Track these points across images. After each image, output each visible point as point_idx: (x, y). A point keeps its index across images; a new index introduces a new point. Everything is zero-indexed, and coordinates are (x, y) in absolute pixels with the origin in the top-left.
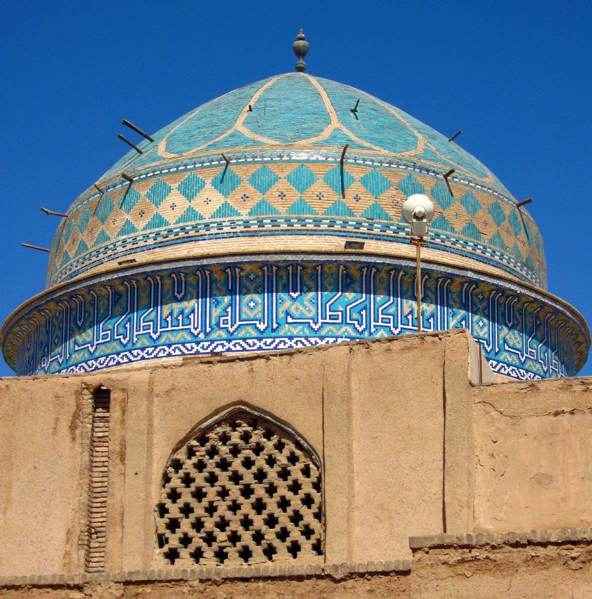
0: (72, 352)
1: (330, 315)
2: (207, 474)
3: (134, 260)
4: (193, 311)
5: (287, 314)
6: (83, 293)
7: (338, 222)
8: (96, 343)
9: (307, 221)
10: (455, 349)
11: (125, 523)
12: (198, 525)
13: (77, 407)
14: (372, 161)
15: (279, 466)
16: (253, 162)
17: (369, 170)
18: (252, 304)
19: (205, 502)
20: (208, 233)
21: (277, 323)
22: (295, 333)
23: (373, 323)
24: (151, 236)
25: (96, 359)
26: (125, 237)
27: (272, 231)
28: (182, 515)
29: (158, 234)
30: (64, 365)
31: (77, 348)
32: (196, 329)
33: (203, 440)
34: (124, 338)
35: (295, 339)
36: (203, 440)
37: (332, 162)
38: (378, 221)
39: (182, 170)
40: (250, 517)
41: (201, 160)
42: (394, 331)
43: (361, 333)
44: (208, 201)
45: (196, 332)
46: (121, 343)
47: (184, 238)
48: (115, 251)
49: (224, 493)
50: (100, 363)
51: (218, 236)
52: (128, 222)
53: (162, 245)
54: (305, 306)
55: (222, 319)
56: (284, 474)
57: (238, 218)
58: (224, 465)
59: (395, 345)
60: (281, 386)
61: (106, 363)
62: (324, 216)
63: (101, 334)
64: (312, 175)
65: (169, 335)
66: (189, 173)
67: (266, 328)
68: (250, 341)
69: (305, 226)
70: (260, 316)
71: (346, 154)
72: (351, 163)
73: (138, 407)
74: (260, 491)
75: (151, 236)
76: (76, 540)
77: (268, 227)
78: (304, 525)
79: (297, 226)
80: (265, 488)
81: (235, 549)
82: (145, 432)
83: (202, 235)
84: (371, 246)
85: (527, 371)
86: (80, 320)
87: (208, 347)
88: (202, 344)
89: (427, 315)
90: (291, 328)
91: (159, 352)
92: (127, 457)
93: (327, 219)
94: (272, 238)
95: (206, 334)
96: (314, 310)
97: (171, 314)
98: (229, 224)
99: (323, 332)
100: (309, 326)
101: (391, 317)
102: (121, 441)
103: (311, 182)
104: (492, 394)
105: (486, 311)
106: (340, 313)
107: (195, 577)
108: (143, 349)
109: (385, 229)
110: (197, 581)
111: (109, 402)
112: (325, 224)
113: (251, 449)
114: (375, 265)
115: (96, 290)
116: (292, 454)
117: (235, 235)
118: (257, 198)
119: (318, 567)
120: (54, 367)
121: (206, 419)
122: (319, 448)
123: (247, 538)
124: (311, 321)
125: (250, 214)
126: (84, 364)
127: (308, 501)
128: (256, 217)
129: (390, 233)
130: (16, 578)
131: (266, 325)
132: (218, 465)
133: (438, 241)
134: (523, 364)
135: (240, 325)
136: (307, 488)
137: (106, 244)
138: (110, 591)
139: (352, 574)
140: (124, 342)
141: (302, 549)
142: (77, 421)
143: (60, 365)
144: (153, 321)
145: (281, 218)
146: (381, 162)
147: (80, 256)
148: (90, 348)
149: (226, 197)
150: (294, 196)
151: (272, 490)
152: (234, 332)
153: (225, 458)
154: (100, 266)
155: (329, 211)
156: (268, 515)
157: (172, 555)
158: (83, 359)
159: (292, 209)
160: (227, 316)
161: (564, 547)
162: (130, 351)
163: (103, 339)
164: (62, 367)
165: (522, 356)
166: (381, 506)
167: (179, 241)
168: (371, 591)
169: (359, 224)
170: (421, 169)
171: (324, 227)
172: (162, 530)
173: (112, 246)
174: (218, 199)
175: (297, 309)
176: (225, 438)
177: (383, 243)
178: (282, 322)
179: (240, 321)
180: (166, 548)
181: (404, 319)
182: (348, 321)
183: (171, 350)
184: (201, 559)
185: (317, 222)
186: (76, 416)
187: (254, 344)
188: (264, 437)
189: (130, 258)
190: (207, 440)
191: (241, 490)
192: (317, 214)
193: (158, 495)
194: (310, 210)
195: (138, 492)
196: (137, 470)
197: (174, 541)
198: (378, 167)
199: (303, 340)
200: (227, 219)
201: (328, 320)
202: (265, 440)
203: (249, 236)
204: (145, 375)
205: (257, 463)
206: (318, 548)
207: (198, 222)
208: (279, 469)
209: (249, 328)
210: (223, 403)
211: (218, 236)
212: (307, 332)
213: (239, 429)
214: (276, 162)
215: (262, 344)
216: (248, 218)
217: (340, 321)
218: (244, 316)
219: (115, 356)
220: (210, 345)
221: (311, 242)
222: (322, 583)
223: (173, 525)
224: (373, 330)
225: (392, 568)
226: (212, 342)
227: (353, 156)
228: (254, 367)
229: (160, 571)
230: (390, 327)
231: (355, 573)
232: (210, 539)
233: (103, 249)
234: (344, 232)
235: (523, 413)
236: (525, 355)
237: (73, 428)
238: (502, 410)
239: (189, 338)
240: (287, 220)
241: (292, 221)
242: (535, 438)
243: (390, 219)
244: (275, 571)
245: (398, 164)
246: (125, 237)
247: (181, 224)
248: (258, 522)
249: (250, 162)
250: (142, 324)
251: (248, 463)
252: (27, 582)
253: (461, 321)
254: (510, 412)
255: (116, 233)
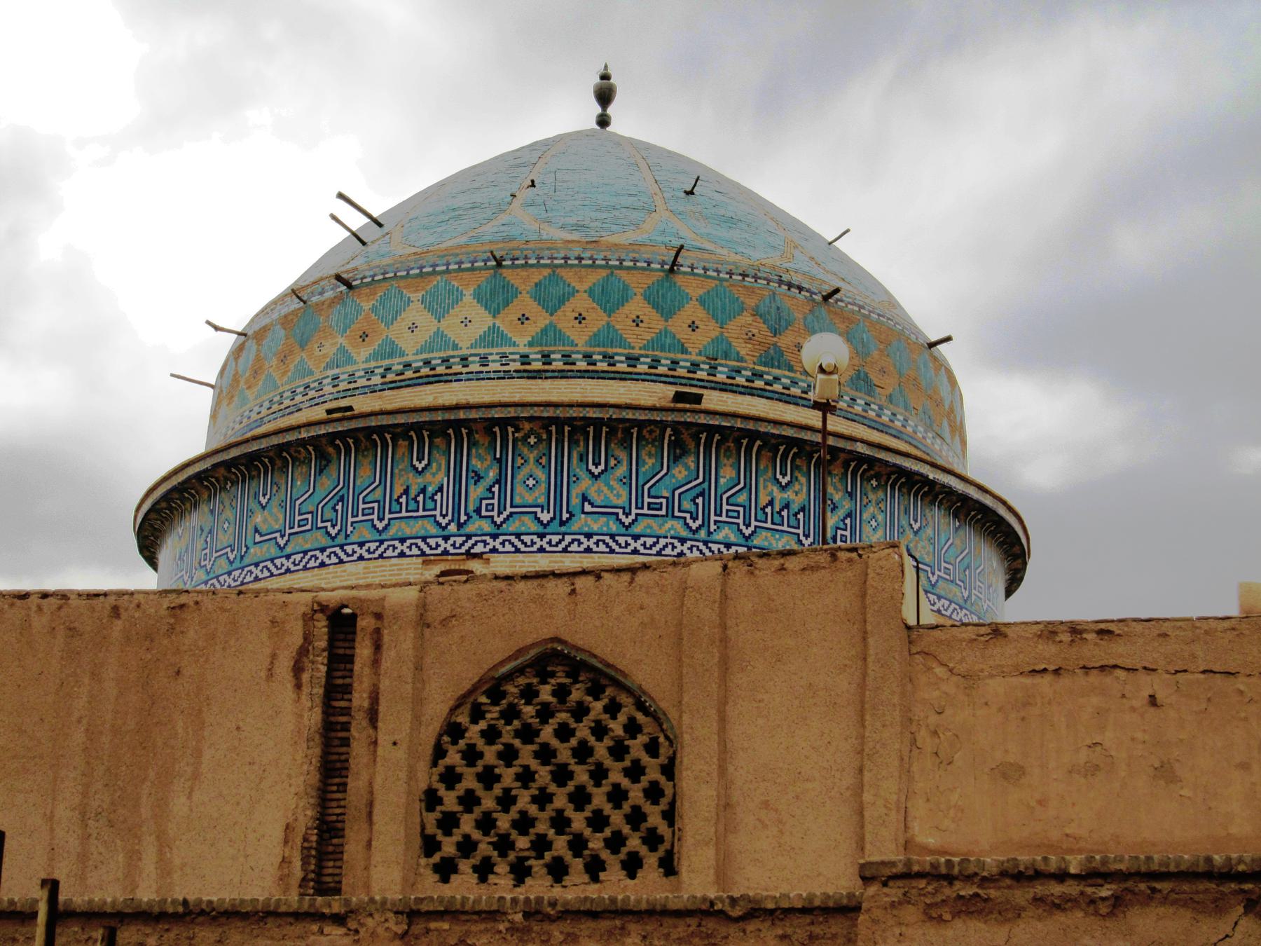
0: (250, 543)
1: (649, 504)
2: (500, 747)
3: (350, 408)
4: (440, 489)
5: (585, 498)
6: (271, 454)
7: (663, 361)
8: (288, 531)
9: (617, 358)
10: (883, 571)
11: (375, 818)
12: (486, 823)
13: (305, 639)
14: (718, 271)
15: (612, 738)
16: (538, 265)
17: (713, 283)
18: (531, 482)
19: (497, 790)
20: (465, 370)
21: (568, 512)
22: (595, 528)
23: (713, 518)
24: (377, 371)
25: (288, 557)
26: (336, 371)
27: (563, 371)
28: (460, 808)
29: (388, 369)
30: (237, 564)
31: (258, 538)
32: (444, 516)
33: (496, 694)
34: (333, 526)
35: (596, 538)
36: (496, 694)
37: (657, 270)
38: (723, 362)
39: (429, 274)
40: (567, 814)
41: (458, 259)
42: (744, 531)
43: (695, 532)
44: (466, 322)
45: (444, 522)
46: (328, 533)
47: (428, 376)
48: (321, 393)
49: (526, 777)
50: (294, 563)
51: (482, 376)
52: (342, 350)
53: (395, 386)
54: (611, 488)
55: (484, 502)
56: (618, 751)
57: (512, 349)
58: (527, 734)
59: (793, 563)
60: (617, 618)
61: (303, 564)
62: (642, 352)
63: (297, 518)
64: (626, 288)
65: (403, 524)
66: (439, 278)
67: (552, 519)
68: (527, 539)
69: (614, 365)
70: (542, 500)
71: (679, 259)
72: (685, 273)
73: (400, 644)
74: (582, 775)
75: (377, 371)
76: (299, 841)
77: (558, 365)
78: (648, 829)
79: (602, 366)
80: (589, 771)
81: (541, 862)
82: (410, 680)
83: (456, 374)
84: (713, 400)
85: (939, 598)
86: (264, 495)
87: (462, 545)
88: (452, 539)
89: (795, 507)
90: (590, 518)
91: (386, 550)
92: (381, 716)
93: (647, 356)
94: (563, 382)
95: (460, 526)
96: (625, 494)
97: (406, 492)
98: (497, 357)
99: (636, 529)
100: (618, 519)
101: (741, 509)
102: (371, 693)
103: (624, 299)
104: (939, 642)
105: (882, 506)
106: (664, 501)
107: (518, 909)
108: (361, 545)
109: (734, 374)
110: (520, 915)
111: (355, 633)
112: (644, 363)
113: (567, 711)
114: (719, 429)
115: (292, 451)
116: (632, 720)
117: (507, 375)
118: (541, 320)
119: (704, 899)
120: (221, 566)
121: (502, 663)
122: (673, 714)
123: (560, 845)
124: (620, 511)
125: (531, 344)
126: (269, 564)
127: (654, 793)
128: (539, 349)
129: (740, 380)
130: (242, 901)
131: (551, 514)
132: (517, 734)
133: (759, 384)
134: (933, 586)
135: (512, 513)
136: (653, 773)
137: (307, 380)
138: (387, 925)
139: (754, 910)
140: (333, 532)
141: (645, 866)
142: (305, 659)
143: (231, 563)
144: (378, 502)
145: (578, 352)
146: (731, 273)
147: (265, 398)
148: (279, 540)
149: (494, 317)
150: (597, 320)
151: (599, 774)
152: (502, 523)
153: (530, 724)
154: (296, 415)
155: (652, 344)
156: (594, 812)
157: (446, 870)
158: (268, 556)
159: (595, 340)
160: (493, 498)
161: (1090, 881)
162: (341, 547)
163: (299, 526)
164: (234, 566)
165: (933, 574)
166: (766, 804)
167: (420, 381)
168: (784, 937)
169: (695, 366)
170: (790, 285)
171: (642, 368)
172: (431, 829)
173: (316, 384)
174: (482, 320)
175: (599, 491)
176: (529, 694)
177: (730, 396)
178: (577, 511)
179: (512, 506)
180: (436, 858)
181: (760, 513)
182: (677, 514)
183: (404, 548)
184: (491, 876)
185: (632, 360)
186: (303, 652)
187: (533, 543)
188: (589, 695)
189: (343, 403)
190: (504, 695)
191: (551, 772)
192: (633, 348)
193: (425, 777)
194: (622, 343)
195: (391, 773)
196: (397, 737)
197: (449, 847)
198: (726, 280)
199: (607, 539)
200: (495, 350)
201: (645, 511)
202: (590, 699)
203: (529, 378)
204: (412, 594)
205: (578, 734)
206: (669, 866)
207: (451, 353)
208: (611, 743)
209: (526, 518)
210: (529, 641)
211: (482, 376)
212: (614, 527)
213: (553, 681)
214: (572, 266)
215: (400, 547)
216: (526, 350)
217: (663, 512)
218: (517, 500)
219: (317, 553)
220: (464, 542)
221: (622, 390)
222: (710, 924)
223: (449, 823)
224: (713, 527)
225: (817, 903)
226: (469, 537)
227: (688, 263)
228: (577, 586)
229: (463, 898)
230: (435, 516)
231: (760, 909)
232: (504, 845)
233: (302, 389)
234: (673, 377)
235: (982, 671)
236: (937, 572)
237: (298, 670)
238: (951, 665)
239: (434, 530)
240: (587, 356)
241: (595, 357)
242: (1000, 709)
243: (740, 359)
244: (638, 901)
245: (756, 278)
246: (336, 371)
247: (425, 356)
248: (578, 822)
249: (532, 266)
250: (361, 506)
251: (564, 733)
252: (260, 908)
253: (845, 518)
254: (961, 668)
255: (323, 365)
